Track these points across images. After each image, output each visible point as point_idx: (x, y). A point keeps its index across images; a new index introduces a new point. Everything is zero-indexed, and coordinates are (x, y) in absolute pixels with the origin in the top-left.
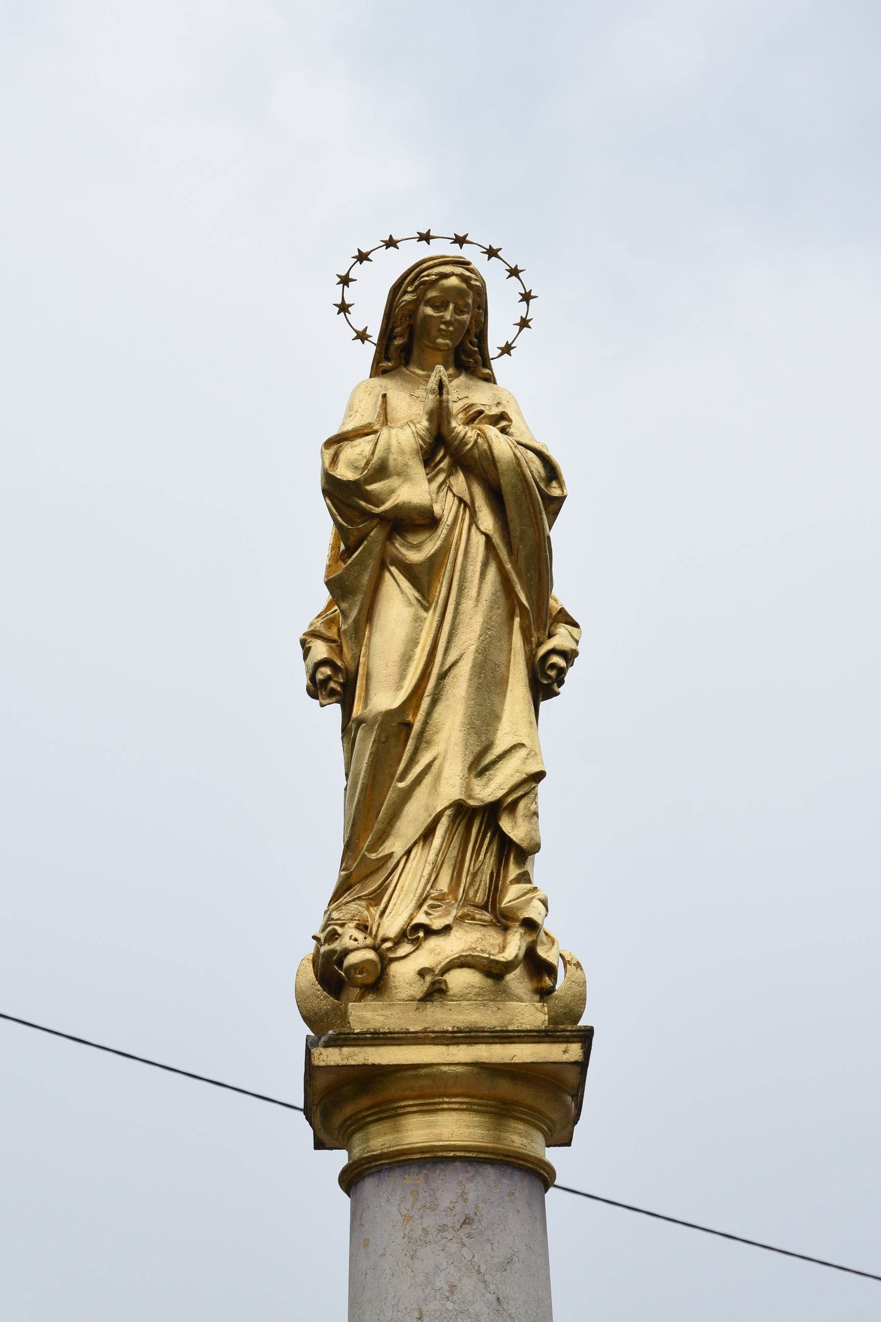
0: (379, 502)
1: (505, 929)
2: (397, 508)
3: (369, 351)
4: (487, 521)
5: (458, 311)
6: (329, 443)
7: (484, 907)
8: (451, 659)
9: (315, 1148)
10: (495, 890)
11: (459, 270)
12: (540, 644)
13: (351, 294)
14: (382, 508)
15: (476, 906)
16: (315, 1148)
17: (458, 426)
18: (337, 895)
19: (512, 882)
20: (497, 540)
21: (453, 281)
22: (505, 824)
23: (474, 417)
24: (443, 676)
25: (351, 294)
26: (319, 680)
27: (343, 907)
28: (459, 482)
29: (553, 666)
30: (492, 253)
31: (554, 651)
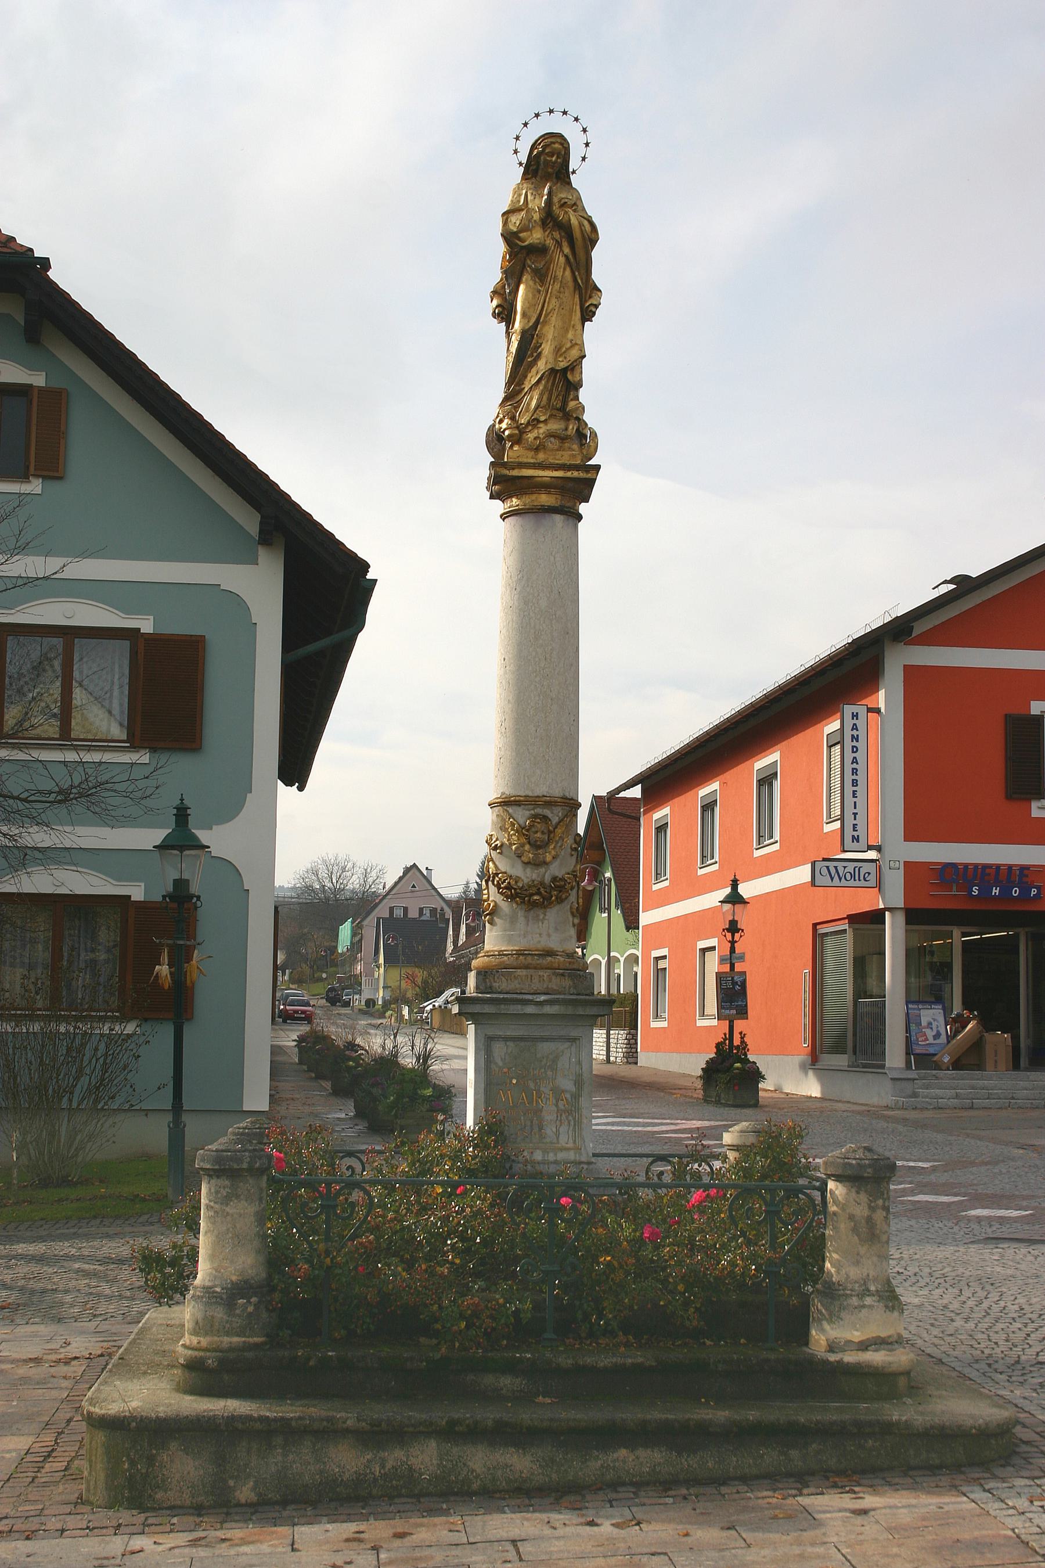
0: (523, 241)
1: (568, 420)
2: (530, 244)
3: (522, 169)
4: (567, 250)
5: (558, 157)
6: (503, 215)
7: (559, 410)
8: (551, 307)
9: (490, 498)
10: (565, 403)
11: (559, 140)
12: (586, 301)
13: (557, 115)
14: (526, 243)
15: (557, 410)
16: (490, 498)
17: (555, 208)
18: (503, 401)
19: (572, 400)
20: (571, 257)
21: (557, 146)
22: (569, 376)
23: (563, 205)
24: (546, 316)
25: (557, 115)
26: (510, 940)
27: (553, 1540)
28: (557, 235)
29: (591, 311)
30: (516, 152)
31: (591, 304)
